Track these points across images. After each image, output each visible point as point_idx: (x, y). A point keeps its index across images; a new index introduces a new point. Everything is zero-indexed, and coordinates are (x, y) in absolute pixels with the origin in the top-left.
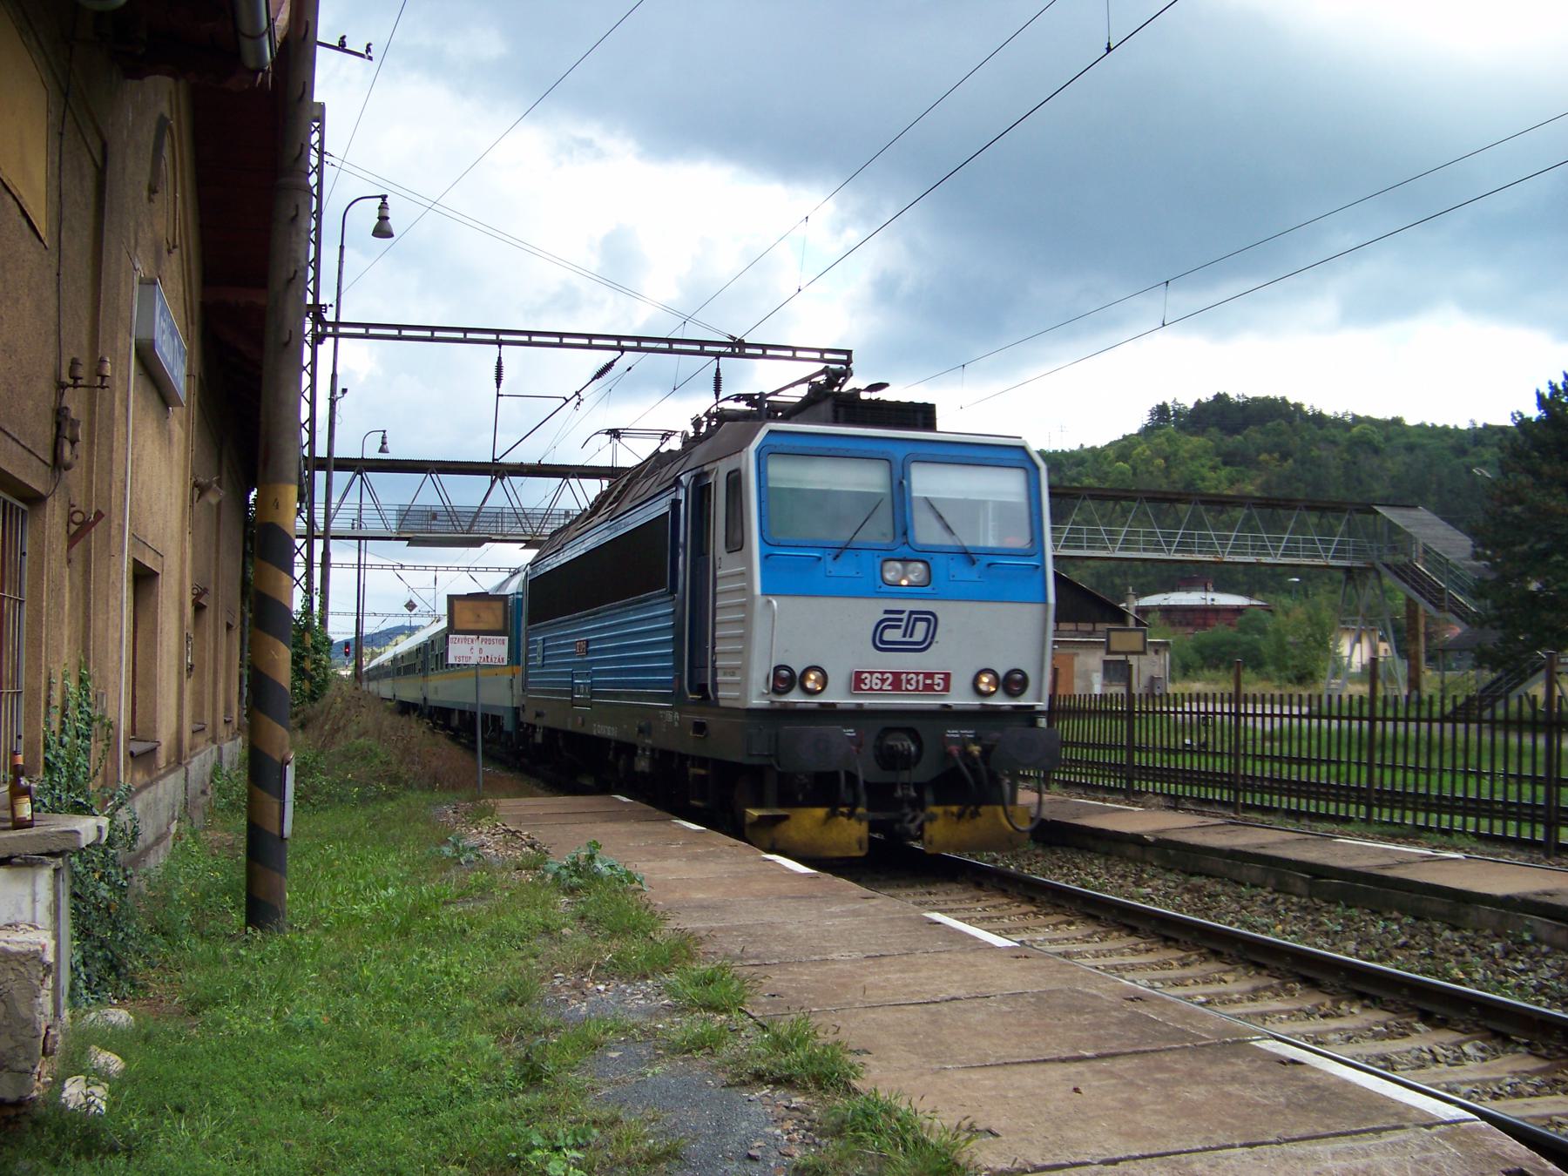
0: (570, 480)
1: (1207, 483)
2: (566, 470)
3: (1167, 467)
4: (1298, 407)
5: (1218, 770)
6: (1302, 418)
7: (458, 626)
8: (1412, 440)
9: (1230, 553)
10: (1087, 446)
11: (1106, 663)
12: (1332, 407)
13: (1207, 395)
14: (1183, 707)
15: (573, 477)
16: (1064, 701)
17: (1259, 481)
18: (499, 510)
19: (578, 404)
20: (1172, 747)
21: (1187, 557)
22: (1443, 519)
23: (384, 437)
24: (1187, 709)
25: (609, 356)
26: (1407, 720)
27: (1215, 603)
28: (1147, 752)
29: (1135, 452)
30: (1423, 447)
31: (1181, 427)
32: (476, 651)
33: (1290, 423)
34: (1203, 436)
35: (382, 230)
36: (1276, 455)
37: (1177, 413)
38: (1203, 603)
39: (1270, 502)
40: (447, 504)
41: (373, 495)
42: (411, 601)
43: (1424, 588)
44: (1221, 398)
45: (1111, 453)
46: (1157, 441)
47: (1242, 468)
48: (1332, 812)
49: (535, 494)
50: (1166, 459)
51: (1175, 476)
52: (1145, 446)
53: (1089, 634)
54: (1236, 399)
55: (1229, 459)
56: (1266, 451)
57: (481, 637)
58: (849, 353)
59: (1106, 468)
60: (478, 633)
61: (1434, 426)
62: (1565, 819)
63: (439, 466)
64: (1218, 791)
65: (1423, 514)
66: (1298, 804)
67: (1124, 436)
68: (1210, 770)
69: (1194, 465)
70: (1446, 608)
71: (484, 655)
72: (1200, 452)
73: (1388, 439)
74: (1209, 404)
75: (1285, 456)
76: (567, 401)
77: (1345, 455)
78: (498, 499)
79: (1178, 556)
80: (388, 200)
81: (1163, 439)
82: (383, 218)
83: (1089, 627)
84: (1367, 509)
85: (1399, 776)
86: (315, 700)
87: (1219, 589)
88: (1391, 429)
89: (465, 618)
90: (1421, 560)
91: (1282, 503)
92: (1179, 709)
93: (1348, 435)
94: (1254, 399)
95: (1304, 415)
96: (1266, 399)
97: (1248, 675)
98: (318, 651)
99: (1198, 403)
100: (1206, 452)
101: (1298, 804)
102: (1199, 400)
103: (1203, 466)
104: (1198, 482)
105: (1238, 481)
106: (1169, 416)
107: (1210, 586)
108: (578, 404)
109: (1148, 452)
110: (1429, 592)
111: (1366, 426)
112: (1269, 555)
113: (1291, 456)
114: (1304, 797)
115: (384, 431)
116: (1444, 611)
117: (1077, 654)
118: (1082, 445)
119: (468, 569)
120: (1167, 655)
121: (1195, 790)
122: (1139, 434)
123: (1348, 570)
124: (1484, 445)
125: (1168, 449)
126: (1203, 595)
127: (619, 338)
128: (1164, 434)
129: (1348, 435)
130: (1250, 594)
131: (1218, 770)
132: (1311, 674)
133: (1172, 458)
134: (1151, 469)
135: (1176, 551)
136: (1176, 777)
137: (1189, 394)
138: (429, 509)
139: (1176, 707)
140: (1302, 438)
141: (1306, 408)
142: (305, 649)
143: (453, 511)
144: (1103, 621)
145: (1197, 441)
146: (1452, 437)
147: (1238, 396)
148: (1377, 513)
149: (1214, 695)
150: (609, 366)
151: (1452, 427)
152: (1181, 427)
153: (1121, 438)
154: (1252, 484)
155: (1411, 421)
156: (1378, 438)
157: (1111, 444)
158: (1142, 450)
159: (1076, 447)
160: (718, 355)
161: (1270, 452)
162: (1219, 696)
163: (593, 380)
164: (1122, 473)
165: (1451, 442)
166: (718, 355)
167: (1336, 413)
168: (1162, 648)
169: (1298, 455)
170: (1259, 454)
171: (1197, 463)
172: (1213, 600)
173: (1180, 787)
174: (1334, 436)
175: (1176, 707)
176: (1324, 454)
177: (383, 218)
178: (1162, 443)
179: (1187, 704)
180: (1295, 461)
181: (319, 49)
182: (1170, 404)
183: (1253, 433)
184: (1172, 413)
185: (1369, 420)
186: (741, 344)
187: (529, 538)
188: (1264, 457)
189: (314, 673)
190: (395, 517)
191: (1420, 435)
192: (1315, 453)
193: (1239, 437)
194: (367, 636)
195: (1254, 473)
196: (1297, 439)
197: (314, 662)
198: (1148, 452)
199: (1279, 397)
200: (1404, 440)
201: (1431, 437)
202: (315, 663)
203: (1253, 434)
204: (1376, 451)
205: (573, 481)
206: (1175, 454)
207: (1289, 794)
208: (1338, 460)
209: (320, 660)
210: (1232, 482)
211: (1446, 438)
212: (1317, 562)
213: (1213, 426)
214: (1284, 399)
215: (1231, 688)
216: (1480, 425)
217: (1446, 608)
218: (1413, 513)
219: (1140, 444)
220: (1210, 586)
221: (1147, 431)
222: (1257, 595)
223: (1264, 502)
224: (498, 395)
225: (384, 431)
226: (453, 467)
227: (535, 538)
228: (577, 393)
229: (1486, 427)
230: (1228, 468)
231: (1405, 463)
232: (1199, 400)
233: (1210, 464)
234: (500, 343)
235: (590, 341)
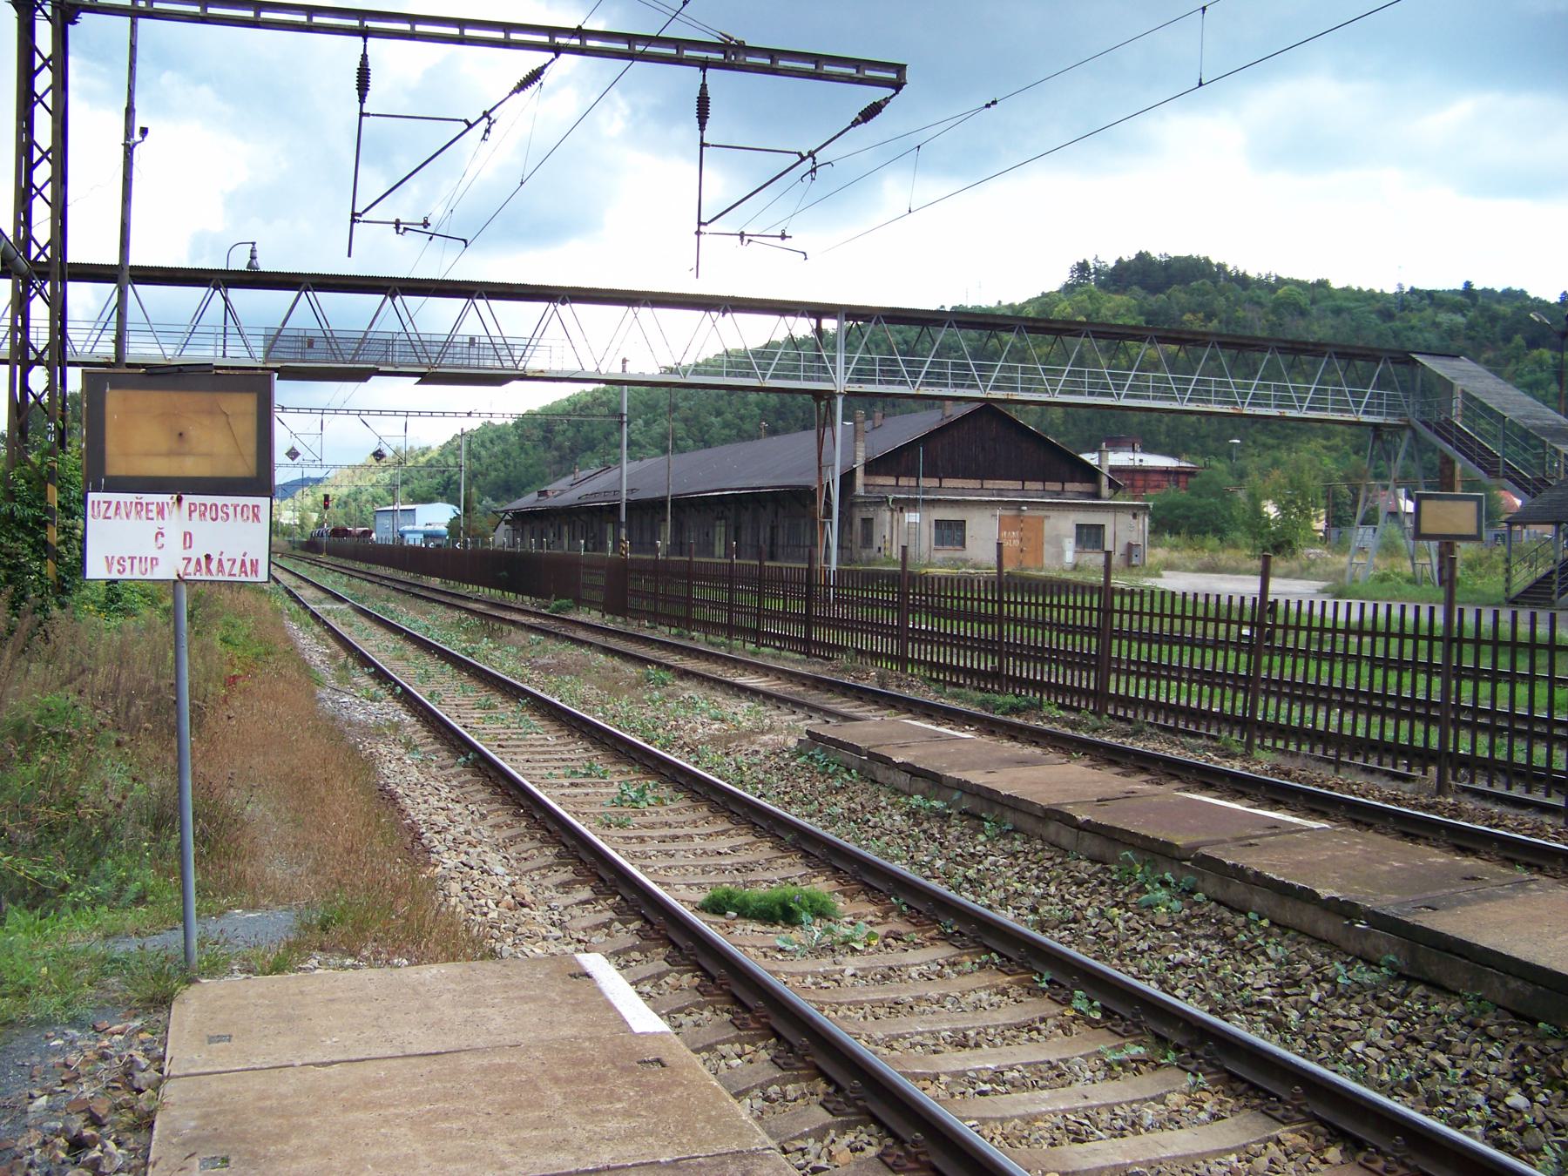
0: (476, 301)
2: (471, 288)
4: (1221, 267)
5: (1337, 684)
6: (1225, 279)
8: (1339, 303)
9: (1250, 404)
10: (1005, 303)
11: (1078, 526)
12: (1255, 268)
13: (1129, 255)
15: (480, 297)
18: (389, 337)
19: (487, 131)
21: (1202, 408)
22: (1490, 371)
23: (253, 251)
25: (539, 58)
27: (1144, 464)
28: (1140, 632)
30: (1349, 310)
31: (1102, 285)
32: (174, 538)
33: (1215, 283)
34: (1123, 293)
36: (1201, 315)
38: (1131, 463)
39: (1296, 346)
40: (325, 327)
42: (293, 448)
43: (1473, 451)
46: (1079, 298)
52: (1066, 303)
53: (1058, 494)
56: (1190, 311)
57: (187, 499)
58: (900, 69)
61: (1360, 290)
63: (316, 281)
65: (1464, 364)
68: (1351, 686)
70: (1501, 474)
71: (197, 552)
72: (1122, 311)
73: (1313, 302)
75: (1209, 317)
76: (470, 126)
77: (1272, 317)
78: (389, 324)
79: (1192, 407)
81: (1085, 297)
83: (1057, 486)
86: (64, 591)
87: (1145, 450)
88: (1317, 290)
90: (1460, 419)
91: (1310, 347)
93: (1274, 296)
94: (1177, 259)
95: (1227, 275)
98: (71, 514)
99: (1119, 261)
100: (1128, 310)
106: (1090, 274)
107: (1137, 446)
108: (487, 131)
109: (1069, 310)
110: (1479, 455)
111: (1293, 287)
112: (1293, 407)
113: (1216, 316)
115: (254, 244)
116: (1497, 477)
117: (1048, 517)
119: (360, 413)
120: (1147, 520)
123: (1376, 426)
124: (1411, 310)
125: (1090, 307)
126: (1131, 456)
127: (552, 31)
128: (1086, 292)
129: (1274, 296)
130: (1172, 454)
131: (1324, 682)
132: (1289, 543)
135: (1190, 400)
137: (1111, 251)
138: (302, 334)
141: (1229, 269)
142: (49, 511)
143: (333, 337)
144: (1072, 481)
146: (1378, 301)
148: (1415, 361)
150: (534, 76)
151: (1378, 291)
155: (1336, 284)
156: (1304, 301)
157: (1029, 302)
159: (993, 304)
160: (704, 65)
161: (1194, 312)
163: (511, 94)
165: (1378, 306)
169: (1223, 316)
170: (1184, 314)
174: (1259, 297)
176: (1250, 315)
178: (1083, 301)
180: (1220, 322)
183: (1178, 294)
185: (1299, 284)
186: (741, 48)
187: (425, 370)
189: (62, 549)
190: (262, 343)
191: (1346, 299)
192: (1240, 313)
193: (1162, 296)
196: (1222, 300)
197: (63, 530)
198: (1069, 310)
199: (1201, 256)
200: (1330, 303)
201: (1357, 300)
202: (64, 532)
204: (1303, 313)
205: (481, 303)
208: (1264, 321)
209: (74, 528)
211: (1373, 302)
214: (1207, 260)
216: (1407, 289)
217: (1501, 474)
218: (1455, 363)
219: (1061, 300)
220: (1137, 446)
221: (1068, 289)
222: (1184, 457)
223: (1289, 345)
224: (362, 114)
225: (254, 244)
226: (332, 281)
227: (433, 370)
228: (486, 115)
229: (1413, 291)
231: (1332, 327)
234: (365, 34)
235: (506, 35)
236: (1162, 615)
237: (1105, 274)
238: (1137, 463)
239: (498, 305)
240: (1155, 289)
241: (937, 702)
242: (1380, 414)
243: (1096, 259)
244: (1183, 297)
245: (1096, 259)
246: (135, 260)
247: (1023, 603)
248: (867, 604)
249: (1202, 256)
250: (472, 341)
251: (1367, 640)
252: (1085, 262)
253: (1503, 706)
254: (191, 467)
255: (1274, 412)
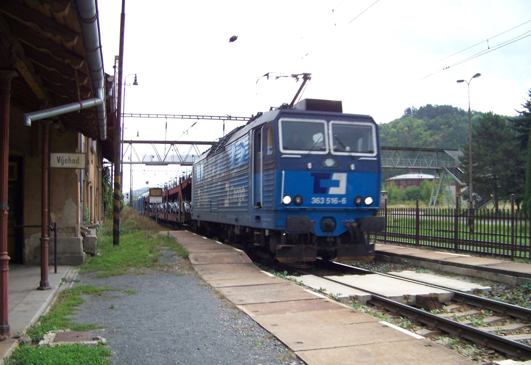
1: (422, 136)
3: (409, 131)
7: (151, 195)
13: (424, 105)
14: (391, 212)
15: (194, 144)
16: (427, 212)
17: (441, 135)
20: (396, 226)
23: (136, 77)
24: (392, 213)
26: (449, 216)
27: (422, 178)
29: (398, 125)
35: (135, 83)
36: (447, 126)
37: (414, 111)
38: (418, 178)
41: (135, 150)
43: (458, 175)
44: (429, 106)
45: (390, 126)
47: (435, 131)
48: (468, 249)
49: (184, 150)
50: (409, 128)
51: (412, 134)
54: (434, 106)
55: (430, 127)
59: (388, 130)
60: (156, 196)
62: (523, 248)
64: (422, 241)
66: (484, 250)
67: (395, 119)
69: (419, 130)
72: (420, 125)
74: (425, 108)
75: (450, 126)
80: (137, 75)
81: (408, 121)
82: (136, 80)
84: (442, 151)
85: (494, 238)
89: (153, 193)
92: (390, 213)
94: (441, 106)
96: (445, 106)
97: (420, 202)
101: (484, 250)
102: (421, 107)
103: (421, 130)
104: (420, 136)
105: (433, 135)
106: (411, 112)
113: (452, 126)
114: (475, 246)
115: (136, 75)
118: (381, 123)
121: (468, 247)
122: (400, 119)
133: (410, 127)
134: (404, 131)
136: (437, 240)
137: (418, 104)
139: (389, 212)
140: (456, 120)
145: (420, 121)
147: (435, 105)
149: (407, 209)
152: (415, 116)
153: (394, 120)
154: (438, 136)
157: (391, 122)
158: (401, 124)
161: (444, 125)
162: (406, 209)
164: (394, 133)
166: (224, 120)
167: (490, 112)
168: (385, 194)
170: (441, 126)
171: (419, 129)
172: (421, 176)
173: (447, 244)
175: (389, 212)
177: (136, 80)
179: (392, 212)
180: (453, 128)
181: (125, 145)
182: (411, 108)
183: (439, 119)
184: (412, 111)
186: (230, 117)
188: (442, 127)
192: (460, 125)
194: (134, 191)
195: (439, 132)
196: (454, 121)
203: (439, 119)
205: (195, 145)
206: (412, 126)
207: (477, 246)
210: (431, 135)
212: (426, 167)
213: (425, 116)
214: (451, 107)
215: (415, 207)
219: (400, 122)
221: (403, 118)
230: (430, 131)
232: (421, 107)
233: (424, 129)
236: (492, 235)
237: (416, 112)
238: (420, 178)
239: (198, 146)
240: (433, 117)
241: (63, 166)
242: (436, 166)
243: (413, 107)
244: (440, 120)
245: (413, 107)
246: (132, 161)
247: (400, 214)
248: (424, 238)
249: (449, 105)
250: (193, 156)
251: (479, 232)
252: (409, 108)
253: (486, 248)
254: (156, 195)
255: (405, 167)
